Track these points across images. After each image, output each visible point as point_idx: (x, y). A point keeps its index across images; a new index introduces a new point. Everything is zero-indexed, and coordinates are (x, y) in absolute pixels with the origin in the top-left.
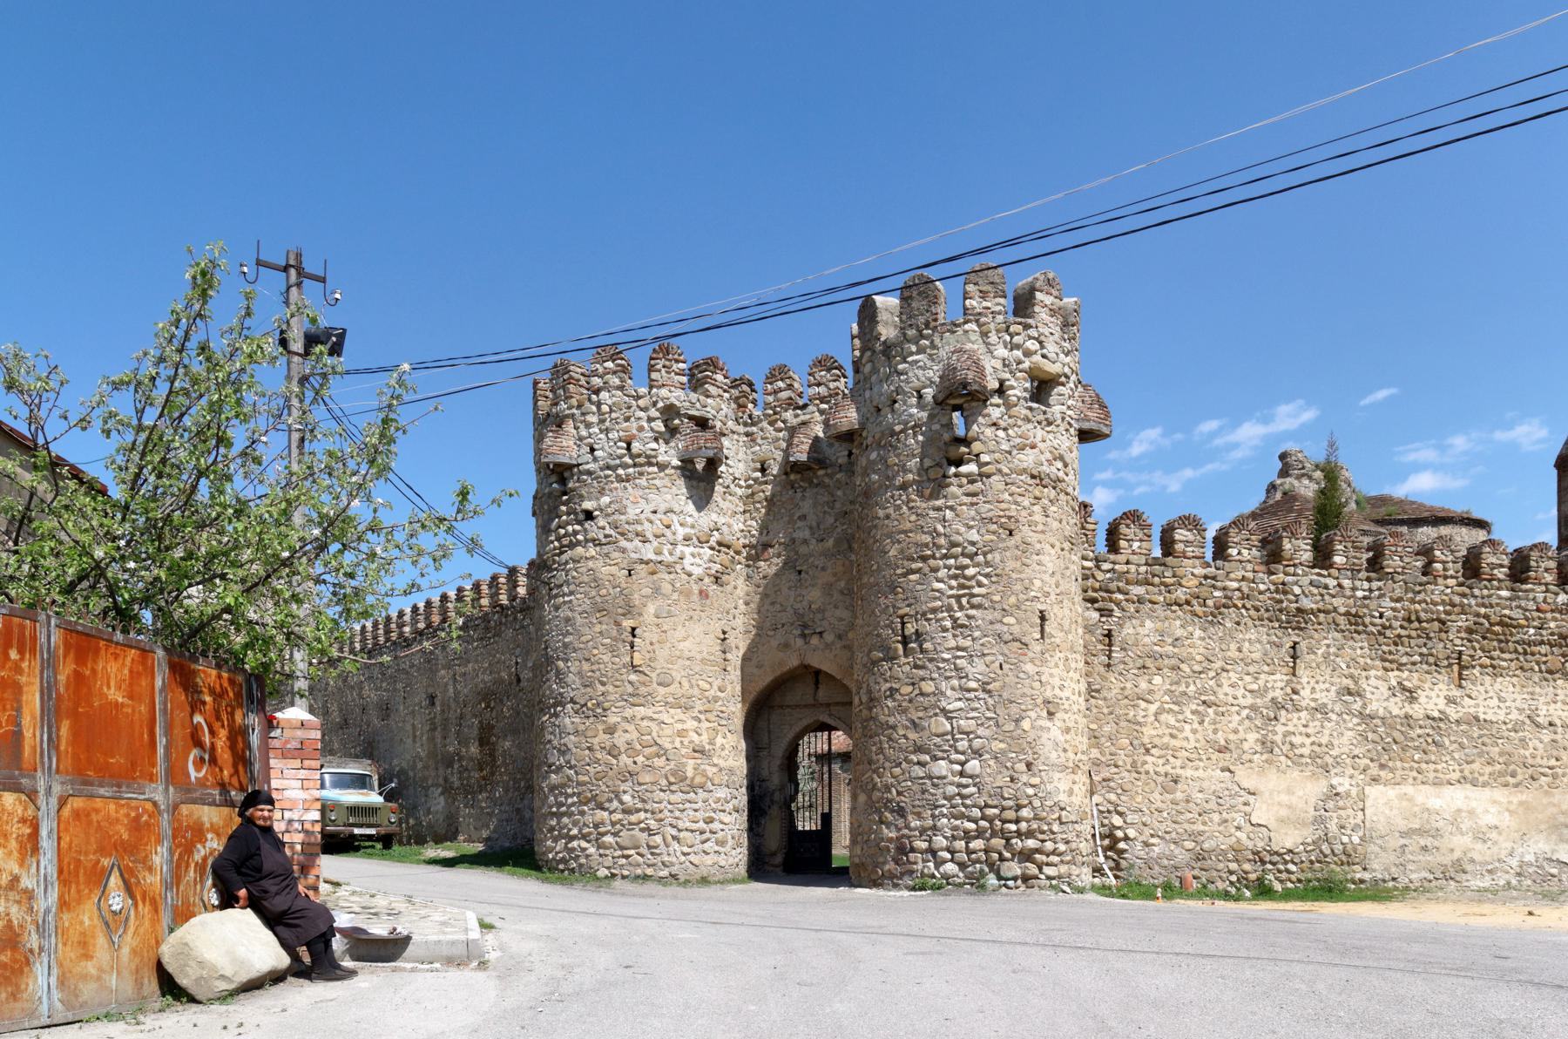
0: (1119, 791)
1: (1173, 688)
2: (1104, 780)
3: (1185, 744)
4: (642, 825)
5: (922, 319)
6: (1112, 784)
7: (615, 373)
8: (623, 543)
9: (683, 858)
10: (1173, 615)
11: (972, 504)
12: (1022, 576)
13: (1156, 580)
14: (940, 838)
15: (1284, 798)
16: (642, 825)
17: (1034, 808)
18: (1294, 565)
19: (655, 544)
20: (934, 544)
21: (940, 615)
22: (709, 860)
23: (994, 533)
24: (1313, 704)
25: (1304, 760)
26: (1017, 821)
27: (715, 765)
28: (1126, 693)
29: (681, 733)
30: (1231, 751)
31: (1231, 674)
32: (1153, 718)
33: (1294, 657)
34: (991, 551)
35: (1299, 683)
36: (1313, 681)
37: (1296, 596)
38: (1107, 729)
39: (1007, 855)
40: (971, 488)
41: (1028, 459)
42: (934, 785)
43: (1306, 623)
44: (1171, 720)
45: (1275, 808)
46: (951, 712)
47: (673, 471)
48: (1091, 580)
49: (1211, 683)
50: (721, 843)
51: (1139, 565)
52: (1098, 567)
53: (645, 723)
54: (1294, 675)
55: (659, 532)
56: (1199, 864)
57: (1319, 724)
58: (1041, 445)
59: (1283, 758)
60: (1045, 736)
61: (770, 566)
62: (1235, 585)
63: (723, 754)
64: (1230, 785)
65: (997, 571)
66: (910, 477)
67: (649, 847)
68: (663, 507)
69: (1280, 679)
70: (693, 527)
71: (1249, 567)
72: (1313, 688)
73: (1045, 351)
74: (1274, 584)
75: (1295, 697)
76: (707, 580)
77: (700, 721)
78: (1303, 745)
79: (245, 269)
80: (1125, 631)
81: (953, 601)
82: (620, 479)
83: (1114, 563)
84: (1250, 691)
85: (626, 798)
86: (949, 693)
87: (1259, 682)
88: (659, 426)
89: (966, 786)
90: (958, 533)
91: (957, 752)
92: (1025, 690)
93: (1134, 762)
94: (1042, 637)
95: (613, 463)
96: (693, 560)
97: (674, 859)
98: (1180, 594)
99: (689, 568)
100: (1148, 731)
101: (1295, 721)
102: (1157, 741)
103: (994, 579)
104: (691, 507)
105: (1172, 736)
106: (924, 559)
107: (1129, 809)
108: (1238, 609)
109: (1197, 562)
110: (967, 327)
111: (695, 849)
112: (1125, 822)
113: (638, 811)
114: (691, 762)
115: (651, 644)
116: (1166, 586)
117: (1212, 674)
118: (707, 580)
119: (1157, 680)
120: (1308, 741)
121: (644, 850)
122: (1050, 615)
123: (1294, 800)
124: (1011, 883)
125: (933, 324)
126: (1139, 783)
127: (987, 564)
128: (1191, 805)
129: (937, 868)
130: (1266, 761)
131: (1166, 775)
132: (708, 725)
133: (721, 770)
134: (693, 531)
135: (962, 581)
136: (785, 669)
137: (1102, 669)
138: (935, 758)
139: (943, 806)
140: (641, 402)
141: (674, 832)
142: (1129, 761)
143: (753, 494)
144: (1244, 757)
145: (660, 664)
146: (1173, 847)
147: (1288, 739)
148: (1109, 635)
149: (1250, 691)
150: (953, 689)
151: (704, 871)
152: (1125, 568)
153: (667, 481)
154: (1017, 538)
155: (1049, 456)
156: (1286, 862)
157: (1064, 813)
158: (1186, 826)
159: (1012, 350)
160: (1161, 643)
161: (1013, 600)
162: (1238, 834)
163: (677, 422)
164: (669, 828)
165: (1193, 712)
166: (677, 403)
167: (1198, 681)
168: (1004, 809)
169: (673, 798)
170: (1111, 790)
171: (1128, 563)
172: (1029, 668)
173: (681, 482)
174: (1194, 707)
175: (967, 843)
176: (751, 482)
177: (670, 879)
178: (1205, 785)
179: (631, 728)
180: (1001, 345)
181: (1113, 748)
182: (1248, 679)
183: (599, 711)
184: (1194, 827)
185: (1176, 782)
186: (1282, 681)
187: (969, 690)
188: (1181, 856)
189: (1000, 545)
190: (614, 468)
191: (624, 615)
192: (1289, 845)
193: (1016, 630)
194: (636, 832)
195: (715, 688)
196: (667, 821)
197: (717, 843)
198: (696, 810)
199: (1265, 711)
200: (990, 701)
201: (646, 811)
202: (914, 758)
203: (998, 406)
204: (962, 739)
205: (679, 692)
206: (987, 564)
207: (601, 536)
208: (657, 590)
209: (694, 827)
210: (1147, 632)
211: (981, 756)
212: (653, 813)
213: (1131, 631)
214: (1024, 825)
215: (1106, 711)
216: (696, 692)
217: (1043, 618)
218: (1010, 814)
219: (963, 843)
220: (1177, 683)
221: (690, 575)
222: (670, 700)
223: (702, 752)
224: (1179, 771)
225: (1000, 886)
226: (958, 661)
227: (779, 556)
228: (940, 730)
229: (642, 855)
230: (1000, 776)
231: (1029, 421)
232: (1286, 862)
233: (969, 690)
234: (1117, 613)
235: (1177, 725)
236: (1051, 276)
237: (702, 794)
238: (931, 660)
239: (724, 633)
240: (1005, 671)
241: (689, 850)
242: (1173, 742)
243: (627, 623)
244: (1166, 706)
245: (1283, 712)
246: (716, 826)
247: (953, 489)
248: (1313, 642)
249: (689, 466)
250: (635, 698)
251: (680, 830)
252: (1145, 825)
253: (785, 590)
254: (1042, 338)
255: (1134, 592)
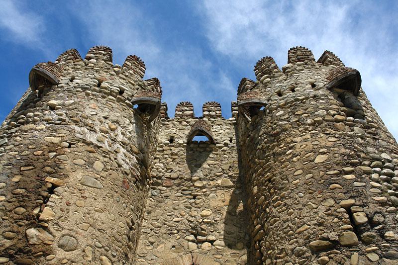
8: (73, 126)
106: (353, 165)
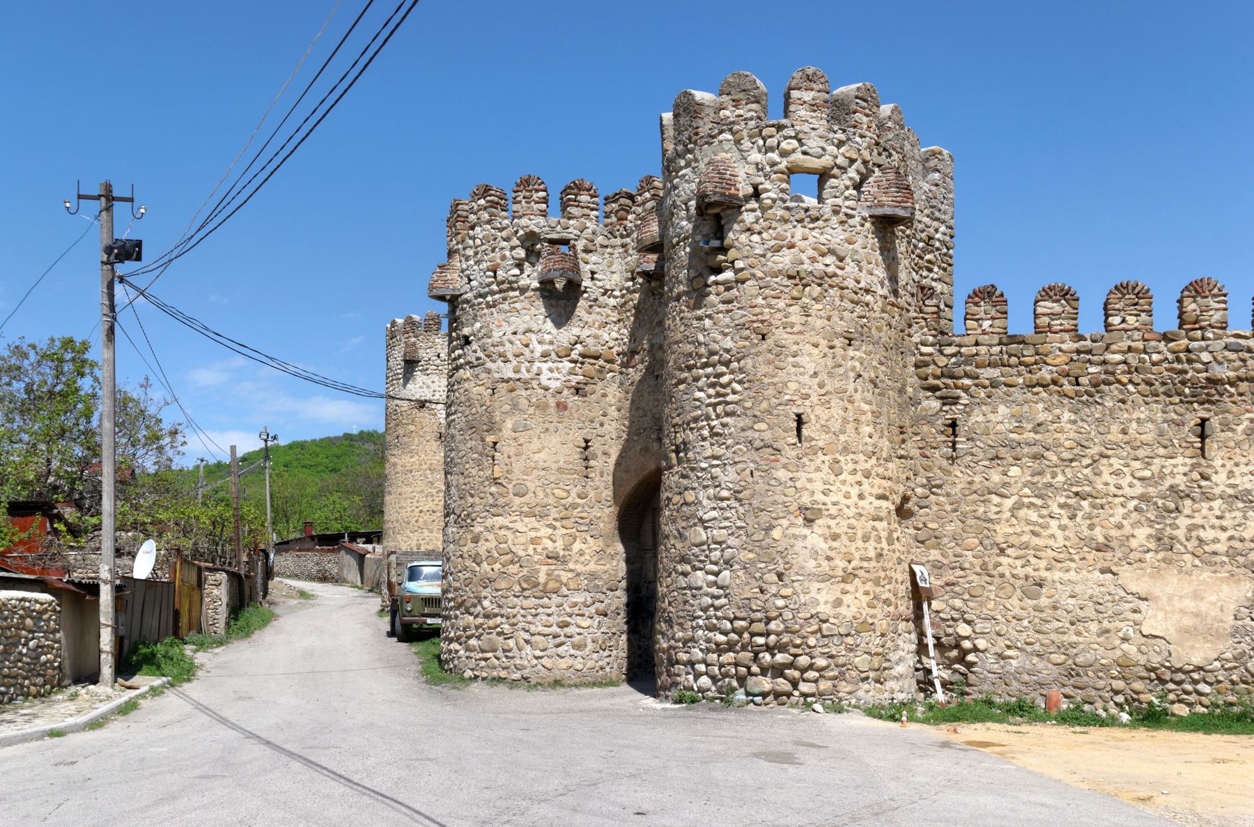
0: (966, 597)
1: (1035, 479)
2: (947, 584)
3: (1051, 542)
4: (499, 629)
5: (686, 134)
6: (957, 589)
7: (485, 209)
8: (489, 365)
9: (535, 662)
10: (1035, 398)
11: (728, 311)
12: (775, 380)
13: (1014, 360)
14: (697, 650)
15: (1189, 604)
16: (499, 629)
17: (784, 621)
18: (1201, 328)
19: (515, 363)
20: (697, 353)
21: (701, 424)
22: (563, 664)
23: (747, 338)
24: (1230, 491)
25: (1217, 559)
26: (768, 634)
27: (571, 571)
28: (974, 488)
29: (534, 541)
30: (1113, 549)
31: (1113, 460)
32: (1009, 514)
33: (1203, 437)
34: (743, 357)
35: (1209, 466)
36: (1229, 465)
37: (1204, 364)
38: (950, 528)
39: (755, 669)
40: (727, 295)
41: (785, 260)
42: (694, 596)
43: (1221, 395)
44: (1033, 516)
45: (1177, 616)
46: (707, 521)
47: (532, 293)
48: (932, 367)
49: (1086, 471)
50: (578, 647)
51: (991, 346)
52: (941, 352)
53: (503, 532)
54: (1204, 457)
55: (518, 352)
56: (1072, 681)
57: (1238, 514)
58: (801, 244)
59: (1188, 557)
60: (799, 544)
61: (635, 374)
62: (1118, 357)
63: (582, 559)
64: (1112, 589)
65: (749, 378)
66: (682, 288)
67: (504, 651)
68: (522, 328)
69: (1182, 463)
70: (551, 343)
71: (1137, 335)
72: (1231, 472)
73: (805, 148)
74: (1174, 352)
75: (1203, 483)
76: (566, 392)
77: (555, 528)
78: (1216, 541)
79: (68, 205)
80: (973, 420)
81: (711, 409)
82: (489, 306)
83: (960, 346)
84: (1140, 479)
85: (486, 603)
86: (705, 502)
87: (1153, 468)
88: (521, 253)
89: (718, 597)
90: (715, 342)
91: (712, 563)
92: (776, 497)
93: (984, 566)
94: (800, 442)
95: (483, 291)
96: (550, 375)
97: (526, 663)
98: (1045, 374)
99: (545, 382)
100: (1002, 530)
101: (1204, 512)
102: (1013, 540)
103: (746, 385)
104: (549, 325)
105: (1034, 533)
107: (979, 617)
108: (1124, 385)
109: (1066, 336)
110: (721, 137)
111: (548, 652)
112: (974, 631)
113: (496, 615)
114: (545, 568)
115: (509, 457)
116: (1027, 365)
117: (1086, 461)
118: (566, 392)
119: (1014, 471)
120: (1223, 536)
121: (500, 653)
122: (810, 416)
123: (1203, 607)
124: (758, 699)
125: (694, 138)
126: (992, 588)
127: (741, 370)
128: (1059, 612)
129: (696, 680)
130: (1164, 560)
131: (1027, 578)
132: (565, 531)
133: (578, 575)
134: (551, 348)
135: (718, 388)
136: (646, 473)
137: (945, 463)
138: (695, 569)
139: (700, 617)
140: (504, 234)
141: (527, 636)
142: (977, 562)
143: (625, 303)
144: (1131, 556)
145: (517, 475)
146: (1035, 660)
147: (1194, 534)
148: (953, 425)
149: (1140, 479)
150: (709, 498)
151: (557, 674)
152: (974, 350)
153: (526, 304)
154: (770, 341)
155: (811, 253)
156: (1195, 682)
157: (824, 626)
158: (1053, 636)
159: (766, 153)
160: (1018, 429)
161: (764, 405)
162: (1125, 646)
163: (539, 246)
164: (522, 633)
165: (1061, 506)
166: (536, 230)
167: (1068, 470)
168: (752, 621)
169: (526, 603)
170: (957, 595)
171: (977, 344)
172: (782, 474)
173: (540, 303)
174: (1062, 500)
175: (719, 656)
176: (625, 292)
177: (522, 681)
178: (1079, 589)
179: (491, 537)
180: (756, 149)
181: (958, 550)
182: (1137, 465)
183: (469, 521)
184: (1065, 638)
185: (1041, 586)
186: (1184, 465)
187: (722, 499)
188: (1046, 670)
189: (753, 351)
190: (483, 296)
191: (487, 431)
192: (1197, 660)
193: (767, 436)
194: (494, 636)
195: (573, 494)
196: (520, 625)
197: (575, 647)
198: (549, 615)
199: (1160, 502)
200: (741, 510)
201: (502, 616)
202: (679, 568)
203: (753, 210)
204: (715, 549)
205: (533, 501)
206: (741, 370)
207: (473, 360)
208: (515, 406)
209: (547, 631)
210: (1000, 419)
211: (732, 566)
212: (508, 618)
213: (980, 419)
214: (773, 638)
215: (948, 508)
216: (551, 500)
217: (800, 420)
218: (758, 627)
219: (715, 656)
220: (1040, 474)
221: (547, 389)
222: (525, 509)
223: (556, 558)
224: (1044, 574)
225: (748, 703)
226: (713, 470)
227: (642, 362)
228: (697, 541)
229: (498, 659)
230: (748, 588)
231: (786, 221)
232: (1195, 682)
233: (722, 499)
234: (965, 399)
235: (1041, 521)
236: (810, 71)
237: (556, 599)
238: (693, 469)
239: (587, 441)
240: (755, 479)
241: (541, 654)
242: (1036, 541)
243: (490, 439)
244: (1026, 500)
245: (1188, 502)
246: (571, 630)
247: (712, 298)
248: (1230, 417)
249: (549, 287)
250: (496, 509)
251: (532, 635)
252: (999, 635)
253: (646, 395)
254: (801, 136)
255: (985, 376)
